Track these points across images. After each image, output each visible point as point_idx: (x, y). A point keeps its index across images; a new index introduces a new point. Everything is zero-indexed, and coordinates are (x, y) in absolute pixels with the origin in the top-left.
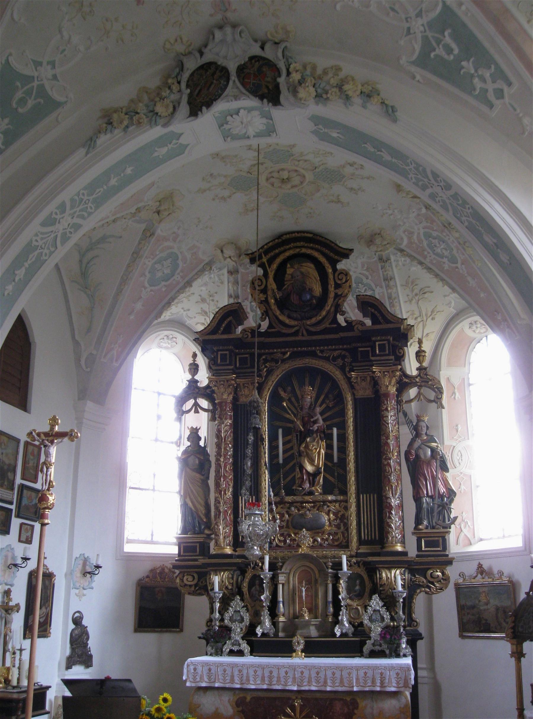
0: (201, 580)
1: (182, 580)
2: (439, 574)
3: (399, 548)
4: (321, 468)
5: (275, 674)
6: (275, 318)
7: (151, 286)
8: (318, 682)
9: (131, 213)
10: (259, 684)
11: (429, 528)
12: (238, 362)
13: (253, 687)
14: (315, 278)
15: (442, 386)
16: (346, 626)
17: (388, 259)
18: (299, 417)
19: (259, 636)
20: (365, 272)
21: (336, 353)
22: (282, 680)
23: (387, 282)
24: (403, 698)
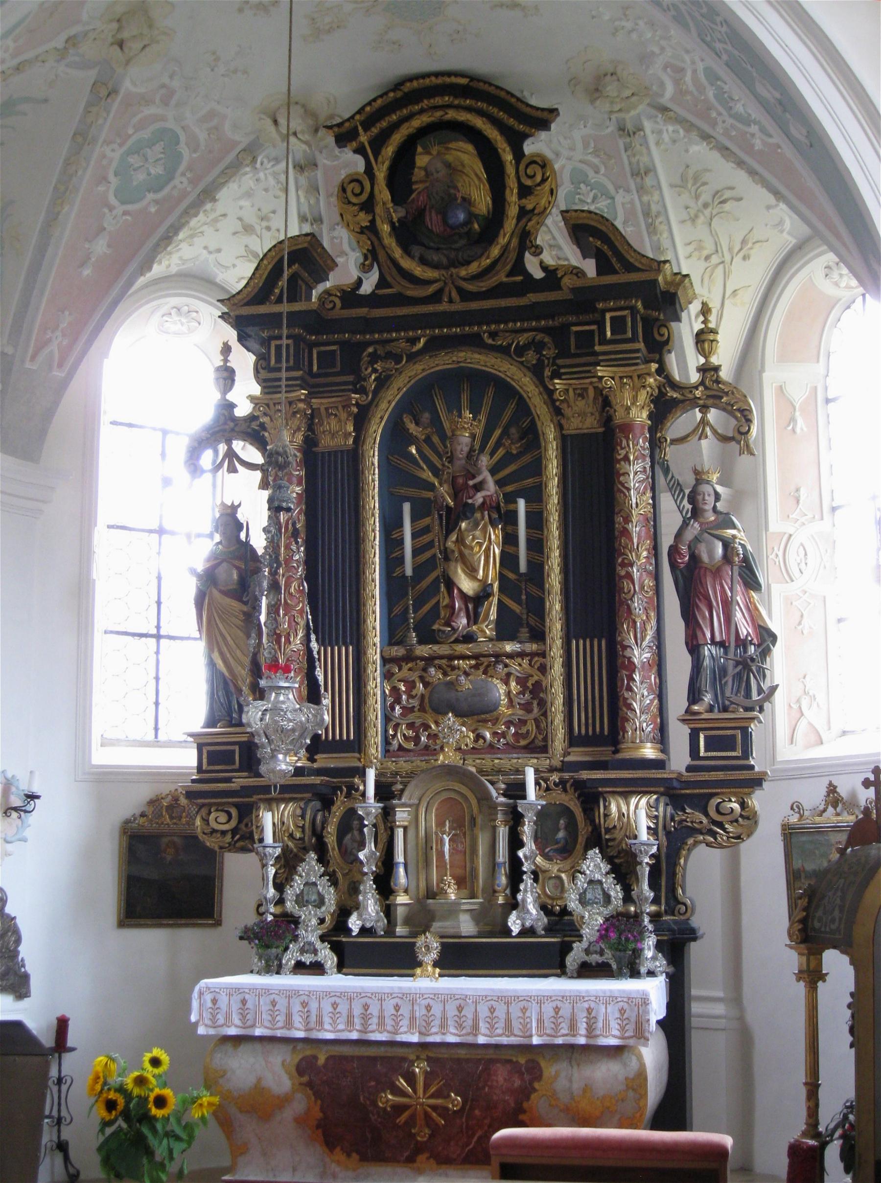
0: (245, 821)
1: (206, 821)
2: (736, 806)
3: (649, 752)
4: (491, 585)
5: (374, 1010)
6: (391, 265)
7: (123, 203)
8: (460, 1026)
9: (55, 48)
10: (343, 1031)
11: (716, 710)
12: (315, 362)
13: (330, 1036)
14: (476, 175)
15: (750, 405)
16: (531, 914)
17: (640, 129)
18: (445, 477)
19: (354, 934)
20: (590, 158)
21: (523, 339)
22: (389, 1022)
23: (638, 180)
24: (634, 1058)
